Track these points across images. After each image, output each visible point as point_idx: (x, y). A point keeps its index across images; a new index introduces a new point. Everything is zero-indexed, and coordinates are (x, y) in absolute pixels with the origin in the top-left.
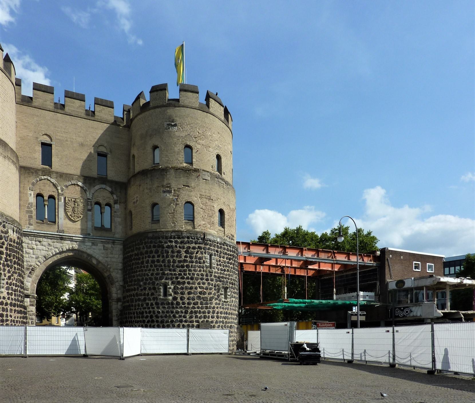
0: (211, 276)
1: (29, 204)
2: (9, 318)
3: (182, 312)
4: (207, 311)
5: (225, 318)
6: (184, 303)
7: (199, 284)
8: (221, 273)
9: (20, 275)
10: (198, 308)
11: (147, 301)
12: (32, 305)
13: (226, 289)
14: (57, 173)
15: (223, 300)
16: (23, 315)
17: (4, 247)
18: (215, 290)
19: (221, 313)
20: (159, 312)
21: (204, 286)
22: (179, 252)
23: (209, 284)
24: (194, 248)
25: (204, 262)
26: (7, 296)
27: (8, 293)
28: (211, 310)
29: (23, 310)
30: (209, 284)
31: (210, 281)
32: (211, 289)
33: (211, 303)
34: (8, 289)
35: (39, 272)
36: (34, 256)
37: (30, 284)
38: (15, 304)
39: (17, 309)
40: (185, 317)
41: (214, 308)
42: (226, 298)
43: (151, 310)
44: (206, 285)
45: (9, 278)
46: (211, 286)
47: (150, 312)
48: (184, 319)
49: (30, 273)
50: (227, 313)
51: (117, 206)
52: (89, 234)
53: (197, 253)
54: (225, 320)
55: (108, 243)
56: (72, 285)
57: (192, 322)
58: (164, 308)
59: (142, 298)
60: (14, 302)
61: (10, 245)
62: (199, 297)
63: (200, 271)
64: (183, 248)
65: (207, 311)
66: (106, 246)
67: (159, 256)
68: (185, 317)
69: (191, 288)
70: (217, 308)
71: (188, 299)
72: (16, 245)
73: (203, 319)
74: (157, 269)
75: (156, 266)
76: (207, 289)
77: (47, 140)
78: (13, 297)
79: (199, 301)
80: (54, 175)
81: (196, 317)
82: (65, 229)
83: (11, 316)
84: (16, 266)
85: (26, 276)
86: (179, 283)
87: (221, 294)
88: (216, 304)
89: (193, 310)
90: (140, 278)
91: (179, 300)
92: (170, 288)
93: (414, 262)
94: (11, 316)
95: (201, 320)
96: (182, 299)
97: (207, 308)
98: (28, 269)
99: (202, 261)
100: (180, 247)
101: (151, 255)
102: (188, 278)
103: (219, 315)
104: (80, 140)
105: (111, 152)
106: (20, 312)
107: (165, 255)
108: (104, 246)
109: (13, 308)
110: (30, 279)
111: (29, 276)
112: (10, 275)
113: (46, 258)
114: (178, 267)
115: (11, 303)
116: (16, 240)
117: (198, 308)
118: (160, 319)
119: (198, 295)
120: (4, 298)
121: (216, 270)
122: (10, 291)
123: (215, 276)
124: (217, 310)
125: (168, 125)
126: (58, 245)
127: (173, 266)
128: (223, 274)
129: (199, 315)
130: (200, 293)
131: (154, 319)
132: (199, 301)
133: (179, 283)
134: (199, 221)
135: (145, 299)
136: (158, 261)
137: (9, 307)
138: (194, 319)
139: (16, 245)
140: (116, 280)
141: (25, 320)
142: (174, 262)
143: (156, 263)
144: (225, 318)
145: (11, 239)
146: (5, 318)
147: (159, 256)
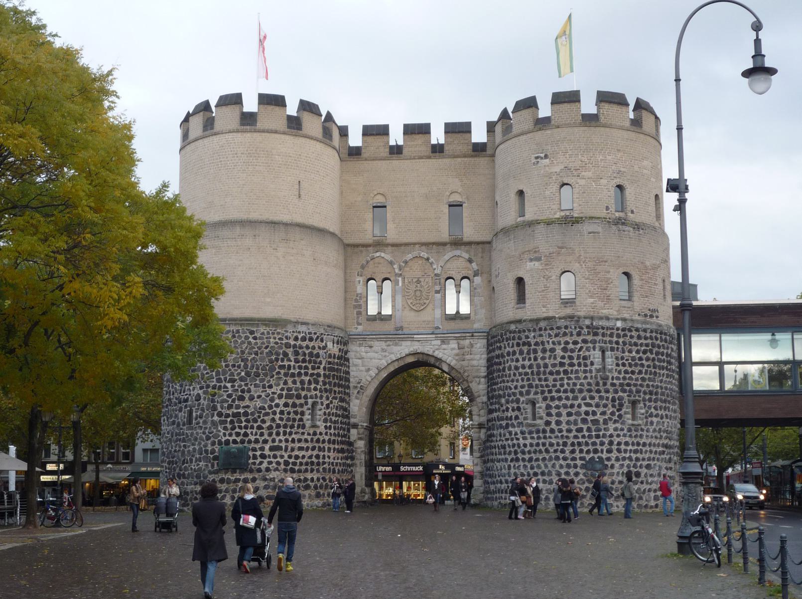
0: (605, 384)
1: (357, 295)
2: (327, 460)
3: (558, 444)
4: (598, 441)
5: (636, 452)
6: (560, 431)
7: (584, 398)
8: (624, 378)
9: (342, 400)
10: (583, 437)
11: (510, 429)
12: (360, 439)
13: (634, 403)
15: (630, 422)
16: (346, 454)
17: (322, 367)
18: (614, 406)
19: (627, 444)
20: (525, 445)
21: (593, 402)
22: (552, 350)
23: (601, 398)
25: (592, 364)
26: (324, 431)
27: (326, 427)
28: (606, 440)
29: (345, 447)
30: (601, 398)
31: (603, 394)
34: (325, 421)
35: (371, 391)
36: (363, 368)
37: (358, 408)
38: (334, 440)
39: (337, 447)
40: (563, 451)
41: (611, 436)
43: (515, 442)
44: (597, 400)
45: (328, 406)
46: (604, 401)
47: (514, 446)
48: (561, 456)
49: (358, 392)
50: (638, 444)
51: (478, 280)
52: (438, 328)
53: (579, 351)
54: (634, 456)
55: (465, 338)
57: (574, 459)
58: (532, 438)
59: (504, 423)
60: (333, 438)
61: (330, 363)
62: (584, 421)
63: (586, 378)
64: (559, 343)
65: (598, 441)
66: (462, 342)
67: (524, 359)
68: (563, 451)
70: (618, 436)
71: (568, 423)
72: (336, 361)
73: (592, 455)
74: (523, 380)
75: (520, 374)
76: (597, 406)
78: (332, 431)
79: (585, 427)
81: (581, 451)
82: (405, 325)
83: (329, 457)
84: (336, 389)
85: (353, 397)
86: (553, 399)
87: (626, 413)
88: (616, 429)
89: (576, 441)
90: (501, 392)
91: (553, 426)
92: (540, 408)
94: (329, 457)
95: (588, 457)
96: (558, 423)
97: (598, 436)
98: (356, 387)
99: (588, 362)
100: (554, 343)
101: (514, 358)
102: (565, 391)
103: (623, 447)
105: (467, 198)
106: (342, 451)
107: (532, 356)
108: (459, 344)
109: (332, 446)
110: (357, 402)
111: (357, 398)
112: (328, 402)
113: (380, 370)
114: (551, 373)
115: (329, 439)
116: (337, 354)
117: (583, 437)
118: (527, 456)
119: (583, 416)
120: (321, 434)
121: (616, 375)
122: (328, 424)
123: (613, 385)
124: (618, 439)
125: (537, 158)
127: (544, 373)
128: (630, 378)
129: (585, 449)
130: (587, 413)
131: (520, 456)
132: (585, 427)
133: (553, 399)
135: (507, 426)
136: (523, 367)
137: (326, 445)
138: (577, 455)
139: (336, 361)
140: (476, 394)
141: (349, 462)
142: (546, 366)
143: (521, 370)
144: (636, 452)
145: (330, 355)
146: (321, 460)
147: (524, 359)
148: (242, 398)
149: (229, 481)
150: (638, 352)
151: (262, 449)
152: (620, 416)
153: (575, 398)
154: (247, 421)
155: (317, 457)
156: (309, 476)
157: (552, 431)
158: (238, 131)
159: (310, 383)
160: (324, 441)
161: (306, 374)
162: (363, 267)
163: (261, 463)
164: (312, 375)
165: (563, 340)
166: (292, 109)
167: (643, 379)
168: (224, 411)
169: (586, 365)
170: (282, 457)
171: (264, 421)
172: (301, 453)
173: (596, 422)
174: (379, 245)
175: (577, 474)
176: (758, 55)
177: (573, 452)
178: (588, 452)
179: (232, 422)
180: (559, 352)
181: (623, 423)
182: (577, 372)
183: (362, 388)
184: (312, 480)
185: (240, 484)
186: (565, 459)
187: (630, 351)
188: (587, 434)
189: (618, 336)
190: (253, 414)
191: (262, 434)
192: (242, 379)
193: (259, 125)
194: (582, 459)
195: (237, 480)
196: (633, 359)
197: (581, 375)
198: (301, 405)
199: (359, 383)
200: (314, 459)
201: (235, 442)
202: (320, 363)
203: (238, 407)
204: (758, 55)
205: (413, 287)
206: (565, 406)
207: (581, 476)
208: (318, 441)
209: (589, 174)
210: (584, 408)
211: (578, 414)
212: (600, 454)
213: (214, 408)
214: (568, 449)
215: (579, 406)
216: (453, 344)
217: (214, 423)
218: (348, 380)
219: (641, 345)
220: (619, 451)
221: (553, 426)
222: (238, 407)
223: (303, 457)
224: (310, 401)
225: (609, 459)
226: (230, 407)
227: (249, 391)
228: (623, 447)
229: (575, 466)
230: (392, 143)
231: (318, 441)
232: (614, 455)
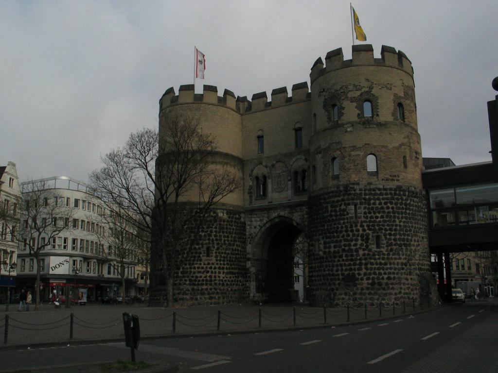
10: (343, 260)
12: (253, 266)
24: (338, 201)
25: (348, 214)
27: (217, 260)
40: (332, 270)
42: (378, 246)
69: (336, 242)
77: (260, 133)
79: (344, 254)
81: (342, 270)
95: (346, 273)
98: (249, 238)
110: (250, 245)
111: (250, 243)
117: (343, 260)
119: (343, 247)
155: (210, 277)
156: (205, 287)
166: (221, 93)
167: (385, 221)
170: (188, 277)
172: (199, 275)
177: (337, 271)
178: (346, 270)
183: (252, 237)
188: (345, 258)
194: (343, 274)
198: (199, 249)
199: (251, 235)
200: (208, 278)
212: (353, 271)
214: (335, 269)
215: (340, 241)
218: (245, 235)
220: (366, 269)
223: (201, 277)
224: (205, 246)
228: (369, 266)
231: (211, 268)
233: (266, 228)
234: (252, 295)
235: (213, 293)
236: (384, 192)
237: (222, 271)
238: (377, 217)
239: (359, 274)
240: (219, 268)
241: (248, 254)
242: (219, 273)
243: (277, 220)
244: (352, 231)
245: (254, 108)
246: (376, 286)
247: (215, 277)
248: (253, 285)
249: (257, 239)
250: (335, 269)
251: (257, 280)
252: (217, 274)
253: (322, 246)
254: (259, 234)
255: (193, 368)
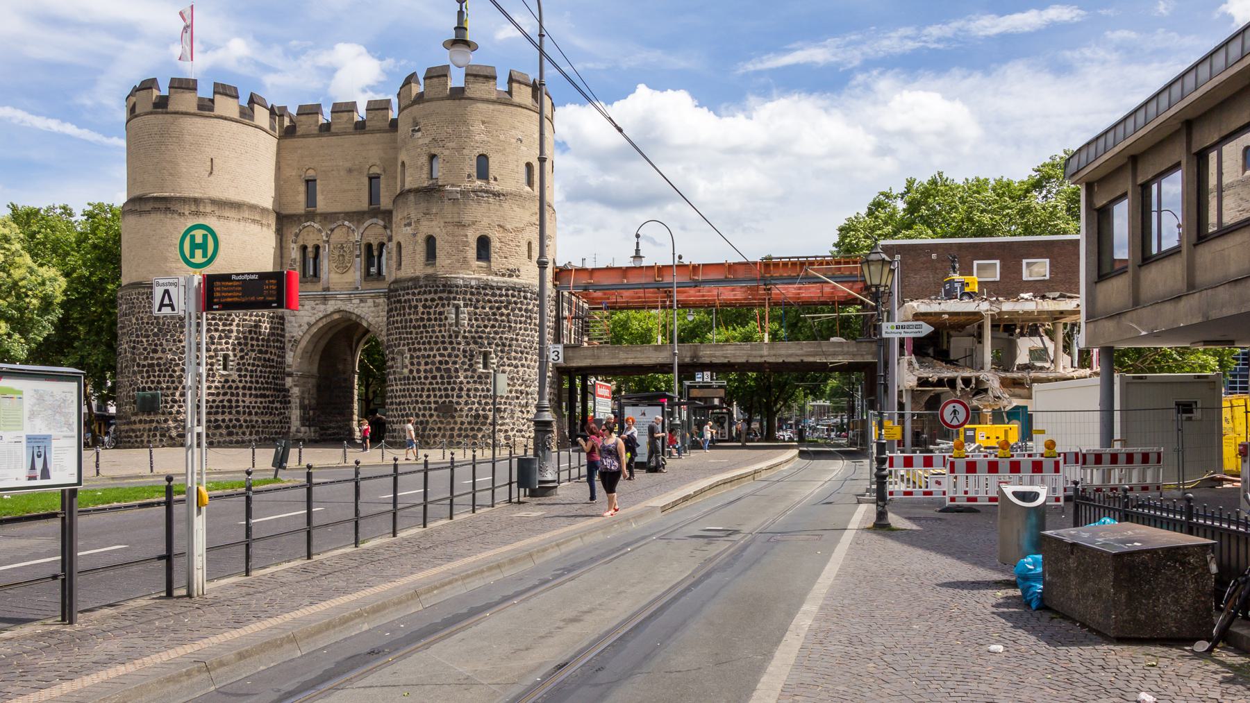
6: (420, 378)
7: (438, 349)
14: (321, 214)
22: (416, 307)
27: (240, 376)
30: (453, 349)
32: (457, 356)
33: (457, 377)
40: (421, 396)
41: (461, 383)
42: (485, 366)
55: (379, 297)
56: (109, 384)
57: (429, 403)
62: (438, 369)
69: (429, 356)
71: (425, 371)
76: (450, 356)
80: (318, 219)
81: (435, 396)
86: (415, 350)
91: (415, 374)
93: (975, 263)
95: (440, 401)
97: (449, 383)
102: (424, 343)
104: (348, 165)
113: (310, 326)
123: (465, 337)
126: (322, 307)
129: (438, 393)
130: (440, 362)
133: (415, 350)
134: (442, 259)
138: (432, 399)
148: (155, 351)
149: (146, 422)
150: (491, 308)
151: (173, 394)
152: (471, 365)
153: (431, 349)
154: (160, 371)
155: (230, 401)
156: (220, 417)
157: (414, 378)
158: (151, 113)
159: (220, 338)
160: (237, 388)
161: (216, 330)
162: (297, 235)
163: (172, 407)
164: (223, 331)
165: (423, 297)
167: (496, 333)
168: (142, 363)
169: (441, 320)
171: (174, 371)
173: (448, 370)
174: (310, 216)
175: (431, 416)
176: (461, 28)
177: (429, 396)
178: (441, 397)
179: (147, 372)
180: (421, 309)
181: (474, 371)
182: (433, 326)
184: (224, 421)
185: (154, 424)
186: (423, 402)
187: (483, 308)
189: (472, 294)
190: (165, 364)
191: (173, 382)
192: (155, 335)
193: (171, 108)
194: (436, 402)
195: (152, 421)
196: (487, 315)
197: (437, 329)
201: (150, 388)
202: (233, 320)
203: (152, 358)
204: (461, 28)
205: (337, 253)
206: (423, 356)
207: (435, 418)
208: (230, 387)
209: (451, 145)
210: (438, 358)
211: (433, 363)
213: (134, 360)
214: (425, 393)
215: (434, 356)
216: (370, 302)
217: (134, 373)
218: (283, 336)
219: (496, 302)
221: (415, 374)
222: (152, 358)
225: (458, 403)
226: (146, 358)
227: (161, 345)
229: (430, 409)
230: (357, 118)
231: (230, 387)
232: (462, 400)
233: (273, 56)
234: (293, 429)
235: (234, 427)
236: (498, 292)
237: (247, 392)
238: (486, 326)
239: (458, 403)
240: (244, 388)
241: (290, 366)
242: (244, 395)
243: (336, 316)
244: (451, 343)
245: (300, 131)
246: (481, 419)
247: (237, 401)
248: (295, 414)
249: (303, 344)
250: (425, 393)
251: (303, 407)
252: (240, 398)
253: (407, 361)
254: (308, 337)
255: (915, 527)
